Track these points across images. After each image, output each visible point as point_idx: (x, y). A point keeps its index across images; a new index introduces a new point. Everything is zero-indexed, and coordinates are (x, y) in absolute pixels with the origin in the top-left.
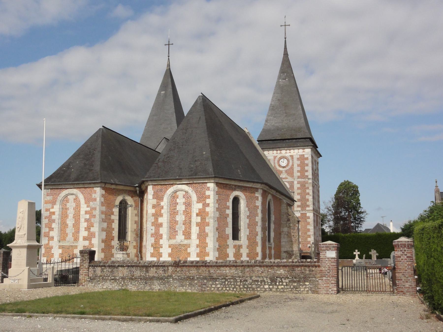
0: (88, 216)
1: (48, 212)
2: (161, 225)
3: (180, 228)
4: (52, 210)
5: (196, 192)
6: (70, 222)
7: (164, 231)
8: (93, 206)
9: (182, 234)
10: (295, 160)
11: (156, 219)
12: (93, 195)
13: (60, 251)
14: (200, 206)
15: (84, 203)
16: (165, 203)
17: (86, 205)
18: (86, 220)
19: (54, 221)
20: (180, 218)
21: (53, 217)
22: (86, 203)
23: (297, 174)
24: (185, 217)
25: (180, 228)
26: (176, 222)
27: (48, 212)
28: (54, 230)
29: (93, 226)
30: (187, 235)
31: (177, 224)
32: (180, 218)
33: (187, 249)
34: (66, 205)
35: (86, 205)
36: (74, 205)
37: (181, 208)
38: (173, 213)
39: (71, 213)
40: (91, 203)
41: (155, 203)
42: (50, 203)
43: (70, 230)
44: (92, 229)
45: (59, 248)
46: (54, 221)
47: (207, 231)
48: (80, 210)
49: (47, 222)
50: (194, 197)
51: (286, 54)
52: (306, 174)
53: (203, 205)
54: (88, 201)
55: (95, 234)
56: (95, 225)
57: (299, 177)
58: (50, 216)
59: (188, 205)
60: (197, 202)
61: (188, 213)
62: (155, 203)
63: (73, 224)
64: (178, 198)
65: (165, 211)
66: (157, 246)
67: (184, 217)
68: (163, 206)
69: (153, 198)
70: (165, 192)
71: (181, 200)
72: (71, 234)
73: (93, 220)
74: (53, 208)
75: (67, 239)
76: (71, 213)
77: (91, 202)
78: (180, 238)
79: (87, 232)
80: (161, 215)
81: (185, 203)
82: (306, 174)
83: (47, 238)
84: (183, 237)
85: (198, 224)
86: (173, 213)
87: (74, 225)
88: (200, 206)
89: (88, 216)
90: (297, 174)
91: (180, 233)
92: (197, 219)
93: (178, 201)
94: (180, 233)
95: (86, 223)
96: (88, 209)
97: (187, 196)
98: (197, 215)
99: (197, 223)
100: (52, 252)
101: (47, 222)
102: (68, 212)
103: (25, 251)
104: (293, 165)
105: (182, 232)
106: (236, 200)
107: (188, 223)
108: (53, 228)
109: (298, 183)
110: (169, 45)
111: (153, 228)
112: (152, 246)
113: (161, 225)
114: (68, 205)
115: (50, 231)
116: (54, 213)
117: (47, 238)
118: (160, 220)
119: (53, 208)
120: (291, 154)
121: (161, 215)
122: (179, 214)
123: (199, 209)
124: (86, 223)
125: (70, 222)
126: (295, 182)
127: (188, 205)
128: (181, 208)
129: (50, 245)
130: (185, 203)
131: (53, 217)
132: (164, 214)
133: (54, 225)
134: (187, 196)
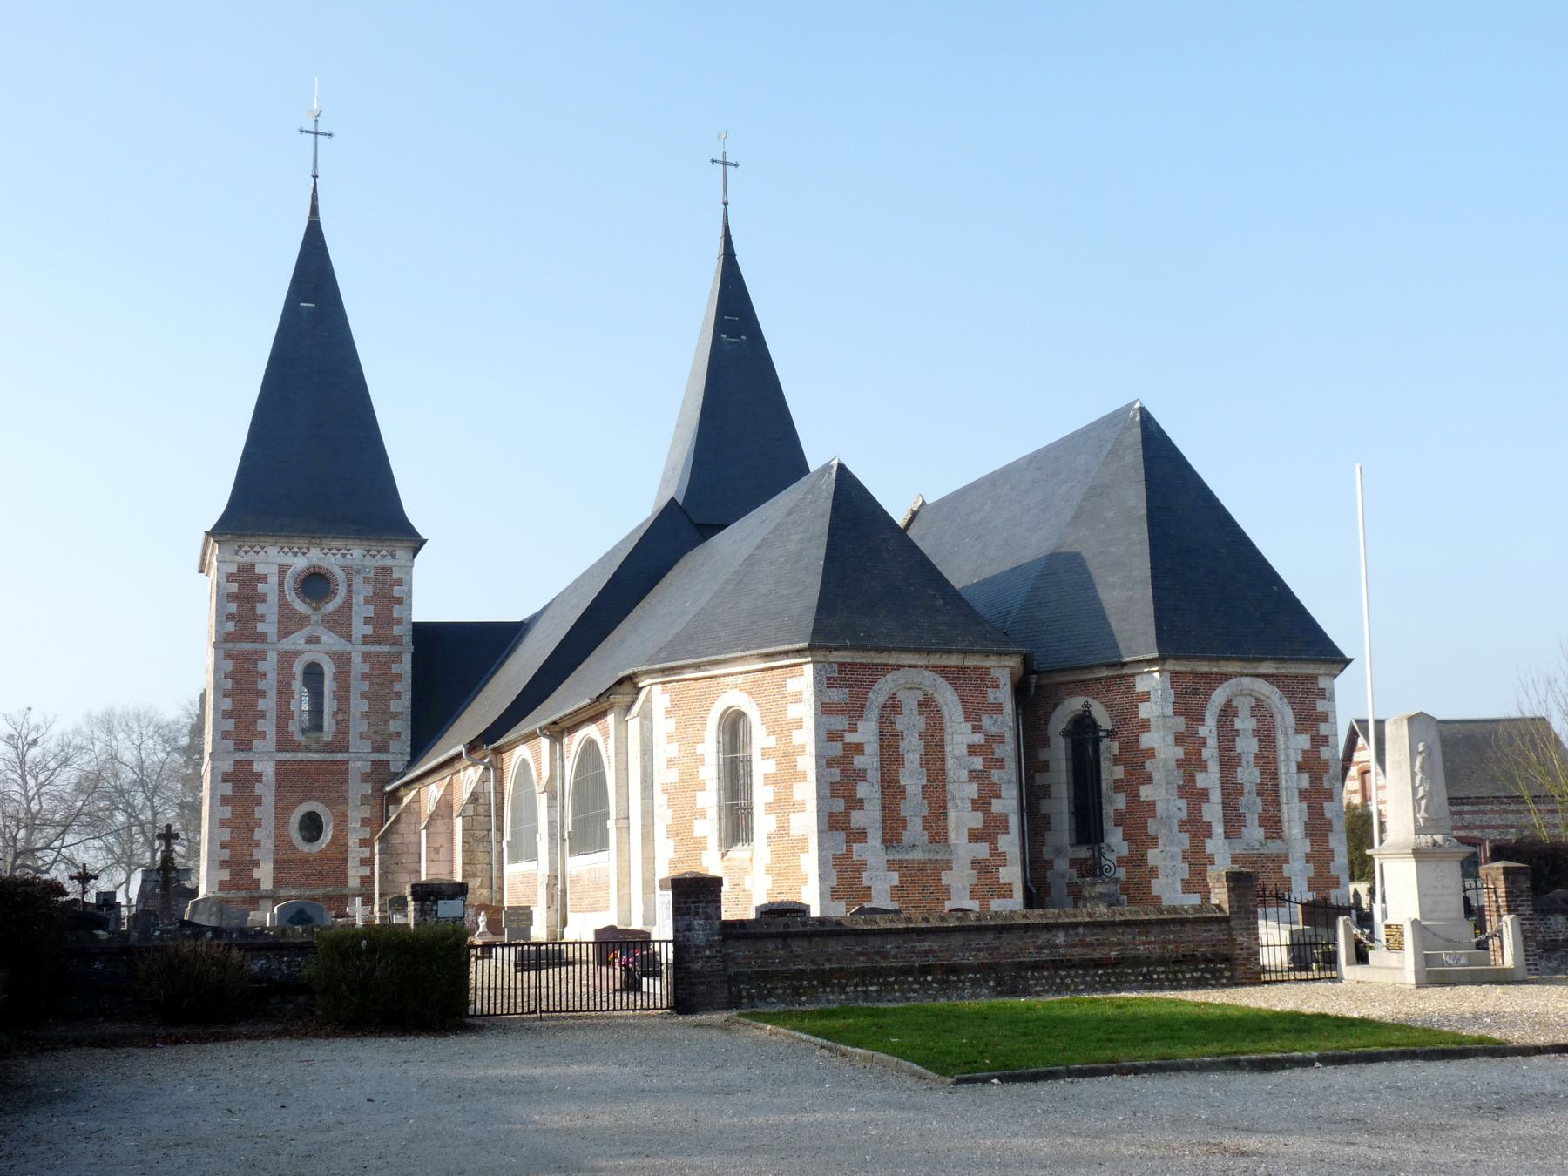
0: (978, 763)
1: (840, 745)
2: (1204, 795)
3: (1251, 805)
4: (850, 738)
5: (1292, 701)
6: (912, 779)
7: (1213, 812)
8: (994, 730)
9: (1256, 822)
10: (358, 581)
11: (1190, 778)
12: (991, 694)
13: (894, 878)
14: (1304, 741)
15: (962, 719)
16: (1208, 728)
17: (969, 725)
18: (974, 776)
19: (862, 775)
20: (1248, 775)
21: (859, 762)
22: (968, 719)
23: (360, 629)
24: (1262, 773)
25: (1251, 805)
26: (1239, 789)
27: (840, 745)
28: (866, 806)
29: (999, 797)
30: (1272, 825)
31: (1242, 794)
32: (1248, 775)
33: (1280, 867)
34: (892, 723)
35: (969, 725)
36: (920, 723)
37: (1247, 746)
38: (1229, 761)
39: (912, 749)
40: (986, 721)
41: (1182, 728)
42: (842, 712)
43: (913, 808)
44: (997, 806)
45: (889, 869)
46: (862, 775)
47: (1328, 815)
48: (942, 740)
49: (838, 779)
50: (1285, 715)
51: (314, 210)
52: (261, 627)
53: (1312, 738)
54: (975, 710)
55: (1006, 820)
56: (1004, 793)
57: (366, 640)
58: (845, 756)
59: (1266, 736)
60: (1297, 732)
61: (1267, 761)
62: (1182, 728)
63: (923, 787)
64: (1236, 715)
65: (1210, 753)
66: (1198, 861)
67: (1257, 772)
68: (1204, 739)
69: (1175, 713)
70: (1208, 696)
71: (1245, 723)
72: (919, 821)
73: (996, 775)
74: (853, 729)
75: (907, 837)
76: (912, 749)
77: (984, 717)
78: (1254, 832)
79: (979, 815)
80: (1203, 767)
81: (1256, 733)
82: (261, 627)
83: (842, 835)
84: (1262, 831)
85: (1303, 795)
86: (1229, 761)
87: (925, 792)
88: (1304, 741)
89: (978, 763)
90: (360, 629)
91: (1252, 820)
92: (1299, 780)
93: (1238, 724)
94: (1252, 820)
95: (975, 786)
96: (978, 739)
97: (1261, 711)
98: (1300, 768)
99: (1300, 791)
100: (866, 883)
101: (838, 779)
102: (903, 745)
103: (1411, 865)
104: (349, 597)
105: (1256, 816)
106: (733, 724)
107: (1270, 790)
108: (861, 801)
109: (366, 657)
110: (316, 133)
111: (1183, 803)
112: (1185, 858)
113: (1204, 795)
114: (900, 723)
115: (849, 808)
116: (859, 748)
117: (842, 835)
118: (1201, 780)
119: (853, 729)
120: (348, 561)
121: (1203, 767)
122: (1244, 763)
123: (1304, 752)
124: (975, 786)
125: (912, 779)
126: (356, 658)
127: (1266, 736)
128: (1247, 746)
129: (855, 857)
130: (1256, 733)
131: (859, 762)
132: (1210, 763)
133: (862, 790)
134: (1261, 711)
